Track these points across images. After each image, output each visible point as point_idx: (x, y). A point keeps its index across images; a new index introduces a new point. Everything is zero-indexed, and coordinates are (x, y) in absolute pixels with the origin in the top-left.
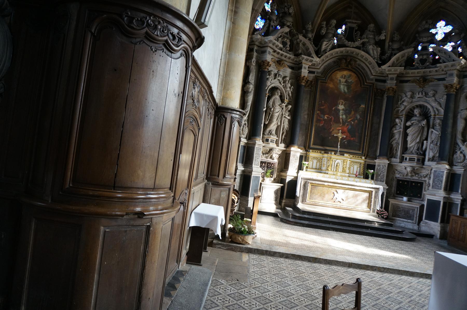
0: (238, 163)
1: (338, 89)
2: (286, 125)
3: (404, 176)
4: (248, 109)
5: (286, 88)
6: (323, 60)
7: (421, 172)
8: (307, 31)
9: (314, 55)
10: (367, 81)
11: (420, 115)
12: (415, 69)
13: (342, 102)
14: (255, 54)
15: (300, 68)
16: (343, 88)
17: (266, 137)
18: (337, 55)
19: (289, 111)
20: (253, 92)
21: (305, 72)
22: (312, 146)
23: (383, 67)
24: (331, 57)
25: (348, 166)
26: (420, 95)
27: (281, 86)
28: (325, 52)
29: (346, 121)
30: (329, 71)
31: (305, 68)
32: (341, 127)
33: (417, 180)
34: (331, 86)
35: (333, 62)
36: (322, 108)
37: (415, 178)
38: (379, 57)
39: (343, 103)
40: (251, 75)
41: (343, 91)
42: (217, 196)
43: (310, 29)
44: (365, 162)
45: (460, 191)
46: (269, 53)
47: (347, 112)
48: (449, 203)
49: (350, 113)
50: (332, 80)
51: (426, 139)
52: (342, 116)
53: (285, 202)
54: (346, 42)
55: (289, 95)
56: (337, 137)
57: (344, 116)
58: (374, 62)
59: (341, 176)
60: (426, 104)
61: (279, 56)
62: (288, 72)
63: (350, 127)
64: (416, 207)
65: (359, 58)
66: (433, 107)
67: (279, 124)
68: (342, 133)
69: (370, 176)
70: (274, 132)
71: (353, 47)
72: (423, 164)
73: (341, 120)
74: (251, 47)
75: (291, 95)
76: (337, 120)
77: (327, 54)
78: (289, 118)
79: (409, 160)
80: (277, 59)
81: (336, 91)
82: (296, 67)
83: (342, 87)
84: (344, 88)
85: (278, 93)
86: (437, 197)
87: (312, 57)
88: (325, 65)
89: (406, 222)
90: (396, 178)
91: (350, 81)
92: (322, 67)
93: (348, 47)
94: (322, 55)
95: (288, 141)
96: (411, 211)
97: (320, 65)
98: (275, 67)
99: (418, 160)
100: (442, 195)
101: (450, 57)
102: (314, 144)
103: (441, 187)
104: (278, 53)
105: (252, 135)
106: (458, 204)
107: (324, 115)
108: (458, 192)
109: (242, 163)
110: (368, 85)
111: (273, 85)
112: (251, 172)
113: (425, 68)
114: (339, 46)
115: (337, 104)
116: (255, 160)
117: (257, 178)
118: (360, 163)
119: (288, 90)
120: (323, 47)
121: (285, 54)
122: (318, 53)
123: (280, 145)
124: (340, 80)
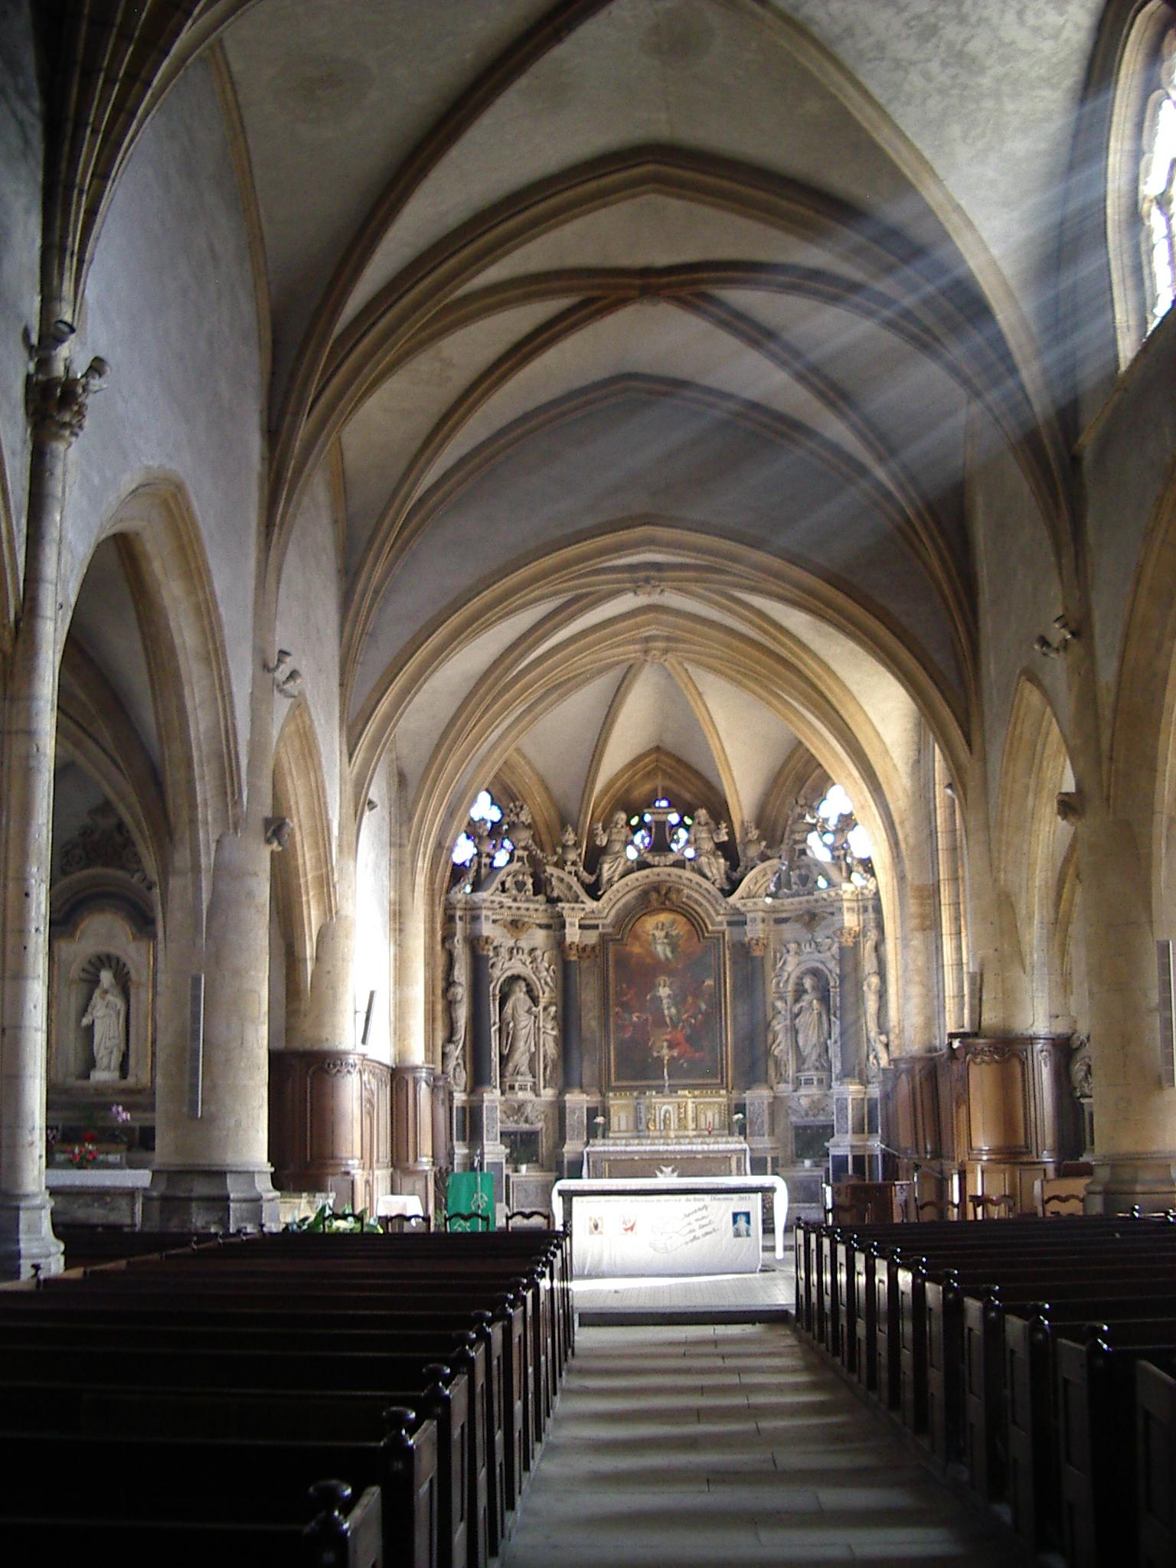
0: (455, 1142)
1: (653, 955)
2: (549, 1047)
9: (584, 897)
10: (710, 928)
11: (813, 988)
15: (563, 926)
16: (662, 950)
17: (508, 1081)
19: (553, 1018)
20: (465, 999)
21: (573, 934)
22: (613, 1084)
25: (690, 1114)
26: (808, 949)
27: (527, 971)
31: (572, 925)
34: (636, 949)
40: (457, 967)
41: (662, 956)
42: (410, 1188)
43: (570, 843)
44: (730, 1099)
46: (487, 917)
47: (678, 1000)
50: (637, 937)
51: (830, 1037)
52: (669, 1011)
54: (650, 858)
55: (546, 983)
56: (660, 1059)
57: (673, 1010)
58: (713, 890)
60: (821, 966)
61: (514, 911)
62: (539, 938)
63: (688, 1031)
65: (685, 882)
67: (533, 1049)
68: (671, 1047)
70: (524, 1068)
72: (830, 1087)
74: (450, 912)
76: (660, 1022)
77: (614, 887)
78: (554, 1033)
80: (509, 918)
82: (556, 925)
83: (659, 948)
88: (617, 906)
95: (560, 1082)
99: (820, 1081)
105: (478, 1080)
109: (464, 1140)
111: (509, 973)
114: (642, 865)
115: (653, 987)
117: (497, 1166)
119: (545, 978)
120: (606, 875)
121: (526, 905)
122: (594, 891)
123: (542, 1092)
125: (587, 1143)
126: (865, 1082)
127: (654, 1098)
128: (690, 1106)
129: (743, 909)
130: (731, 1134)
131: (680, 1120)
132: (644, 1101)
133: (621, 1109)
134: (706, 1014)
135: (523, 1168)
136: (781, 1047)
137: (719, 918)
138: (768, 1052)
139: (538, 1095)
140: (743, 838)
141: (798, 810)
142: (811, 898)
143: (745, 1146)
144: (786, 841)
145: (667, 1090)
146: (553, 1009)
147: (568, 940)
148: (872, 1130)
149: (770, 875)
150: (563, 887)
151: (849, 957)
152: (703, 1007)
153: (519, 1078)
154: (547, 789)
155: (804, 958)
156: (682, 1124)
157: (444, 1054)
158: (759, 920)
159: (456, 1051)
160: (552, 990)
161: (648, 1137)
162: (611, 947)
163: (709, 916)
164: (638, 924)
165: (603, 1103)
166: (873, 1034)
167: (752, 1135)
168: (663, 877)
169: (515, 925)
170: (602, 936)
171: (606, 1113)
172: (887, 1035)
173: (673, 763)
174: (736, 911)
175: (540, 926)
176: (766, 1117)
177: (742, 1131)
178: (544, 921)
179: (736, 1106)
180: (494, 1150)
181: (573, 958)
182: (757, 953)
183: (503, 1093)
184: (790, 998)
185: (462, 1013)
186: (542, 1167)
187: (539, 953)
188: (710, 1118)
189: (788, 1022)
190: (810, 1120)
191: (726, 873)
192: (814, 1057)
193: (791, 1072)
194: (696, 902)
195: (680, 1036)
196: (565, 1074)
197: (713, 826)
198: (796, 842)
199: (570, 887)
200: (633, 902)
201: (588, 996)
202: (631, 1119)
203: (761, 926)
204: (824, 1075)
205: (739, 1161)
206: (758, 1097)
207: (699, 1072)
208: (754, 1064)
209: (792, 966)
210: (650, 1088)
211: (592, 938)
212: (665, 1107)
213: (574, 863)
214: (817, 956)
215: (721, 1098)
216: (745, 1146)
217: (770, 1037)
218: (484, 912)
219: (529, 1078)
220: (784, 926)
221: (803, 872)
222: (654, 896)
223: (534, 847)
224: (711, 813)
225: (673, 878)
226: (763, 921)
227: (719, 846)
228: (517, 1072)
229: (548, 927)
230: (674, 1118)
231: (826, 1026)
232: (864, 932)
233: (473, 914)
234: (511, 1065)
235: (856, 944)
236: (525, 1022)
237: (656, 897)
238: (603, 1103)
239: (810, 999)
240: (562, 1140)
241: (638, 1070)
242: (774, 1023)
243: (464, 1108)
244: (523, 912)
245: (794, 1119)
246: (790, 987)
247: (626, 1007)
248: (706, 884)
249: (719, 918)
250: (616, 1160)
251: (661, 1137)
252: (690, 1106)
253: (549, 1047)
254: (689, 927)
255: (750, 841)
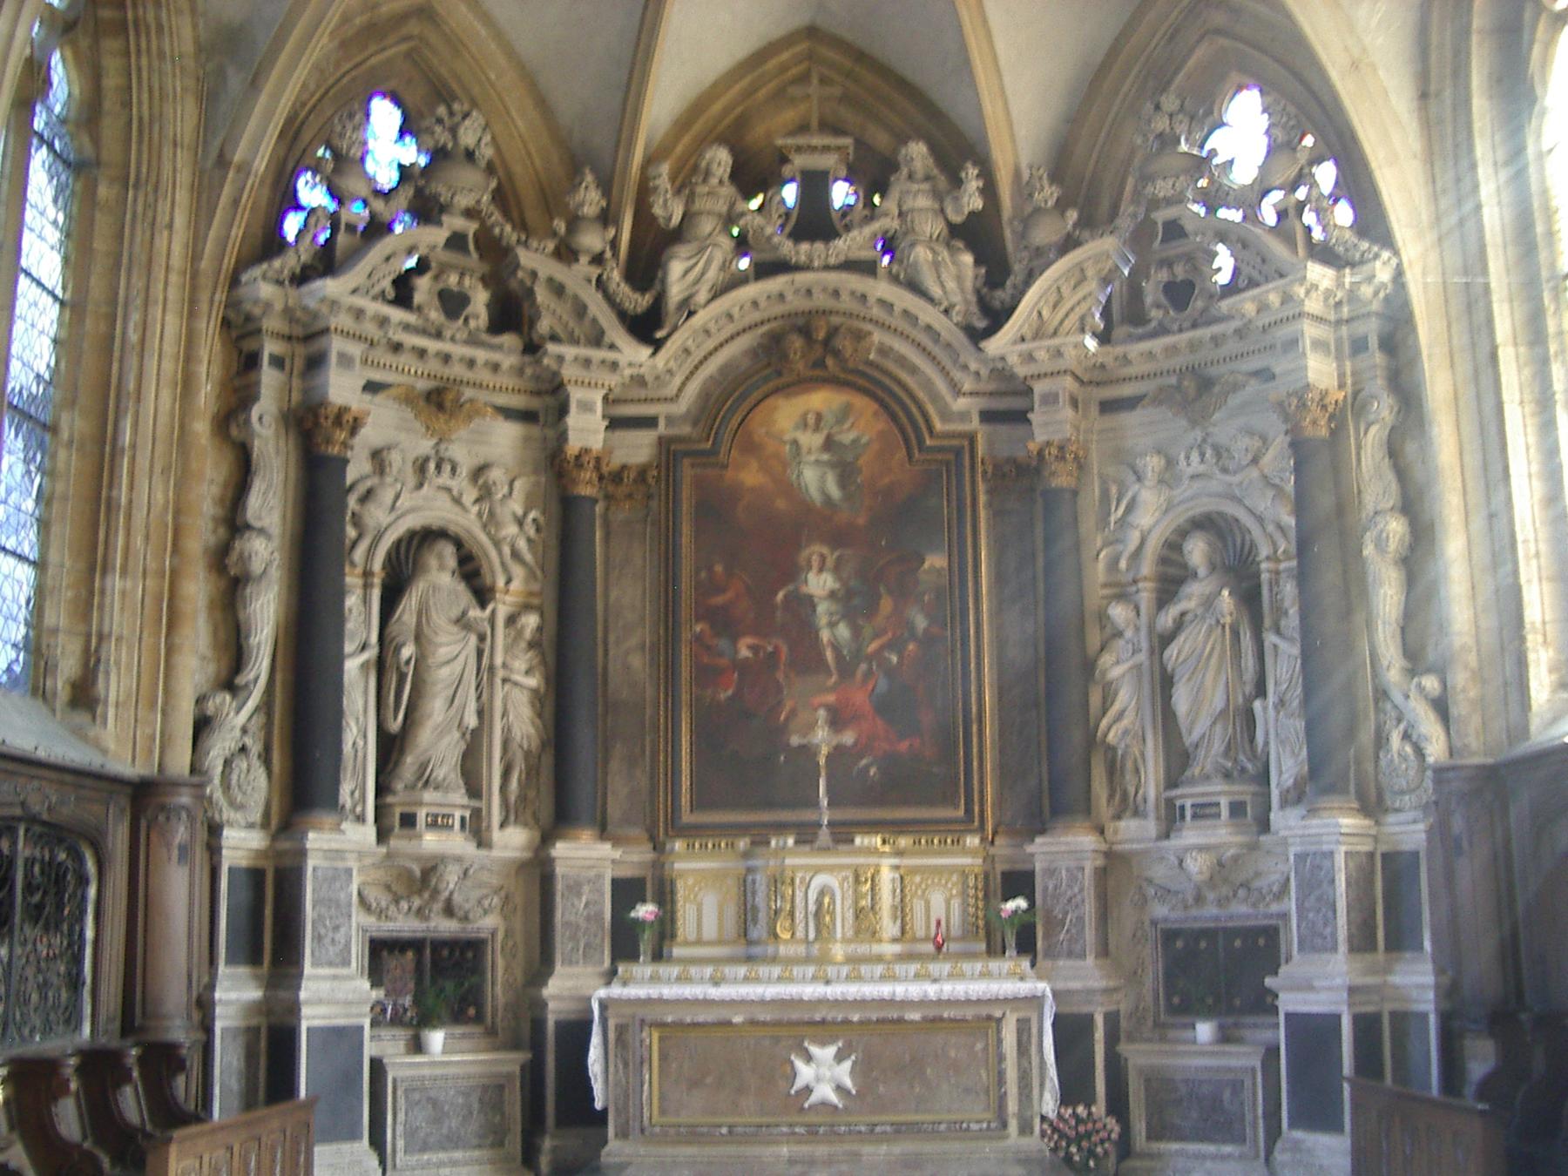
0: (222, 968)
1: (792, 490)
3: (1186, 907)
4: (259, 668)
5: (498, 525)
6: (687, 351)
7: (1258, 874)
8: (574, 222)
9: (616, 332)
10: (938, 426)
11: (1213, 568)
12: (1154, 335)
13: (823, 558)
14: (269, 378)
16: (816, 480)
17: (398, 801)
18: (756, 316)
19: (532, 645)
21: (586, 429)
22: (687, 817)
23: (996, 345)
24: (730, 329)
26: (1196, 465)
27: (466, 521)
28: (688, 309)
29: (858, 655)
30: (733, 400)
31: (586, 407)
32: (833, 689)
33: (1248, 916)
34: (751, 476)
35: (746, 353)
36: (719, 600)
37: (1241, 911)
38: (973, 298)
39: (830, 562)
40: (258, 488)
44: (989, 859)
45: (1427, 945)
47: (855, 603)
48: (1393, 1014)
49: (872, 609)
50: (752, 448)
51: (1261, 690)
52: (832, 631)
53: (554, 1149)
55: (516, 555)
56: (808, 751)
57: (843, 631)
58: (947, 328)
59: (852, 960)
60: (1231, 509)
61: (434, 366)
62: (503, 441)
63: (882, 685)
64: (1244, 1070)
65: (876, 312)
66: (1260, 520)
67: (471, 721)
68: (837, 721)
69: (1011, 940)
70: (446, 766)
71: (827, 268)
72: (1264, 825)
73: (829, 655)
74: (469, 567)
75: (528, 557)
76: (807, 657)
77: (697, 321)
79: (1195, 816)
80: (423, 385)
81: (781, 504)
82: (545, 407)
84: (822, 479)
85: (440, 557)
86: (1323, 996)
87: (612, 347)
89: (1214, 1157)
90: (1154, 923)
91: (847, 438)
92: (693, 387)
93: (797, 268)
94: (675, 329)
95: (546, 809)
96: (1227, 1095)
97: (678, 381)
98: (417, 425)
99: (1237, 809)
100: (1339, 981)
101: (1264, 261)
102: (956, 807)
103: (1334, 935)
104: (422, 353)
105: (304, 787)
106: (1423, 1016)
107: (734, 639)
108: (1421, 947)
109: (254, 958)
110: (940, 449)
112: (294, 1009)
113: (1194, 326)
115: (791, 572)
116: (318, 938)
118: (964, 874)
119: (512, 533)
120: (675, 292)
122: (646, 327)
123: (497, 835)
124: (795, 442)
125: (610, 976)
126: (1372, 805)
127: (788, 854)
128: (887, 876)
129: (1022, 371)
130: (995, 950)
131: (858, 913)
132: (765, 863)
133: (702, 885)
134: (928, 640)
135: (436, 1039)
136: (1124, 717)
137: (961, 404)
138: (1092, 741)
139: (482, 841)
140: (1017, 208)
141: (1161, 124)
142: (1204, 333)
143: (1043, 987)
144: (1127, 208)
145: (824, 836)
146: (531, 621)
147: (574, 445)
148: (1400, 940)
149: (1092, 285)
150: (564, 310)
151: (1316, 457)
152: (921, 622)
153: (429, 796)
154: (542, 103)
155: (1185, 490)
156: (864, 919)
157: (203, 726)
158: (1063, 399)
159: (238, 719)
160: (531, 575)
161: (774, 960)
162: (687, 471)
163: (935, 397)
164: (757, 416)
165: (658, 866)
166: (1394, 673)
167: (1051, 954)
168: (821, 301)
169: (438, 402)
170: (663, 442)
171: (665, 895)
172: (1441, 671)
173: (848, 64)
174: (1001, 373)
175: (508, 413)
176: (1089, 909)
177: (1026, 945)
178: (517, 401)
179: (1006, 876)
180: (334, 992)
181: (586, 490)
182: (1061, 478)
183: (382, 835)
184: (1146, 596)
185: (266, 612)
186: (495, 1038)
187: (496, 475)
188: (938, 911)
189: (1143, 657)
190: (1209, 913)
191: (977, 292)
192: (1218, 746)
193: (1151, 783)
194: (902, 361)
195: (860, 698)
196: (561, 792)
197: (942, 182)
198: (1155, 203)
199: (581, 310)
200: (746, 363)
201: (624, 595)
202: (731, 910)
203: (1068, 413)
204: (1244, 791)
205: (1023, 1027)
206: (1065, 852)
207: (904, 790)
208: (1054, 770)
209: (1150, 515)
210: (781, 828)
211: (637, 448)
212: (819, 880)
213: (598, 259)
214: (1218, 482)
215: (967, 855)
216: (1043, 987)
217: (1095, 699)
218: (337, 345)
219: (459, 797)
220: (1130, 419)
221: (1180, 272)
222: (797, 342)
223: (497, 216)
224: (935, 150)
225: (846, 303)
226: (1074, 403)
227: (954, 231)
228: (424, 779)
229: (527, 416)
230: (843, 921)
231: (1249, 662)
232: (1358, 403)
233: (309, 346)
234: (410, 762)
235: (1338, 432)
236: (451, 656)
237: (801, 350)
238: (658, 866)
239: (1208, 596)
240: (542, 964)
241: (748, 781)
242: (1106, 659)
243: (255, 876)
244: (457, 370)
245: (1160, 910)
246: (1147, 567)
247: (725, 624)
248: (928, 314)
249: (961, 404)
250: (679, 1025)
251: (807, 960)
252: (887, 876)
253: (518, 716)
254: (882, 424)
255: (1038, 210)
